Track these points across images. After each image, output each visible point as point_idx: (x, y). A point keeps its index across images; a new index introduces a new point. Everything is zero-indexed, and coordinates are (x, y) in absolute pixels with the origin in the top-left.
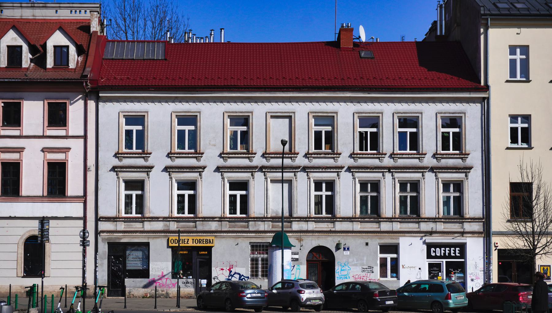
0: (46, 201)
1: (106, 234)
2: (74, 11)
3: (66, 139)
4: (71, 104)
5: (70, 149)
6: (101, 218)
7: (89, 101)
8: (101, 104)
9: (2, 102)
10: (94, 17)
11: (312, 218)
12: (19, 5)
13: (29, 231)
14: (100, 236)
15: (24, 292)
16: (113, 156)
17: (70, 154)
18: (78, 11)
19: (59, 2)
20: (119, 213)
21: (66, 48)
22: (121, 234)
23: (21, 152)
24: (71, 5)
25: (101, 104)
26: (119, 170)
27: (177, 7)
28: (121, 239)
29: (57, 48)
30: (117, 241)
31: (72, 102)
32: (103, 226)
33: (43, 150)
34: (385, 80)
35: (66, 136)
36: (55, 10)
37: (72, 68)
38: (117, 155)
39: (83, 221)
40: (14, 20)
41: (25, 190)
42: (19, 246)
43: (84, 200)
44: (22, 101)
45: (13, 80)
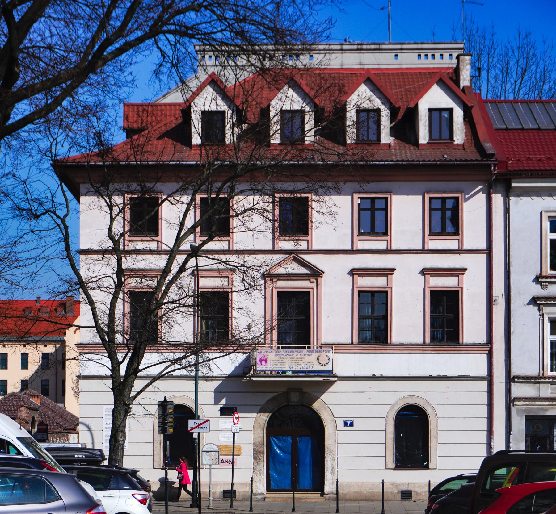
0: (430, 352)
1: (523, 403)
2: (423, 55)
3: (458, 255)
4: (466, 200)
5: (465, 269)
6: (514, 377)
7: (494, 195)
8: (512, 199)
9: (359, 198)
10: (465, 64)
11: (545, 378)
12: (339, 47)
13: (404, 398)
14: (513, 405)
15: (398, 492)
16: (533, 281)
17: (466, 277)
18: (430, 55)
19: (400, 42)
20: (543, 370)
21: (448, 112)
22: (547, 403)
23: (389, 276)
24: (420, 46)
25: (512, 199)
26: (543, 302)
27: (552, 47)
28: (547, 410)
29: (207, 115)
30: (541, 414)
31: (467, 196)
32: (518, 390)
33: (423, 272)
34: (524, 162)
35: (458, 250)
36: (394, 54)
37: (459, 143)
38: (540, 280)
39: (486, 382)
40: (440, 71)
41: (396, 336)
42: (388, 422)
43: (488, 349)
44: (389, 196)
45: (381, 163)
